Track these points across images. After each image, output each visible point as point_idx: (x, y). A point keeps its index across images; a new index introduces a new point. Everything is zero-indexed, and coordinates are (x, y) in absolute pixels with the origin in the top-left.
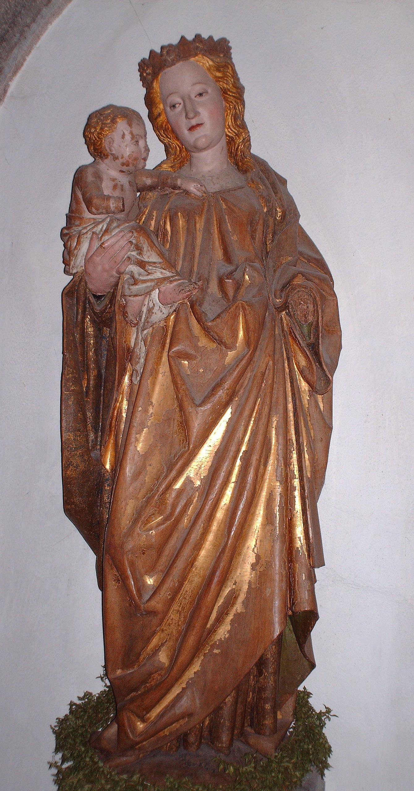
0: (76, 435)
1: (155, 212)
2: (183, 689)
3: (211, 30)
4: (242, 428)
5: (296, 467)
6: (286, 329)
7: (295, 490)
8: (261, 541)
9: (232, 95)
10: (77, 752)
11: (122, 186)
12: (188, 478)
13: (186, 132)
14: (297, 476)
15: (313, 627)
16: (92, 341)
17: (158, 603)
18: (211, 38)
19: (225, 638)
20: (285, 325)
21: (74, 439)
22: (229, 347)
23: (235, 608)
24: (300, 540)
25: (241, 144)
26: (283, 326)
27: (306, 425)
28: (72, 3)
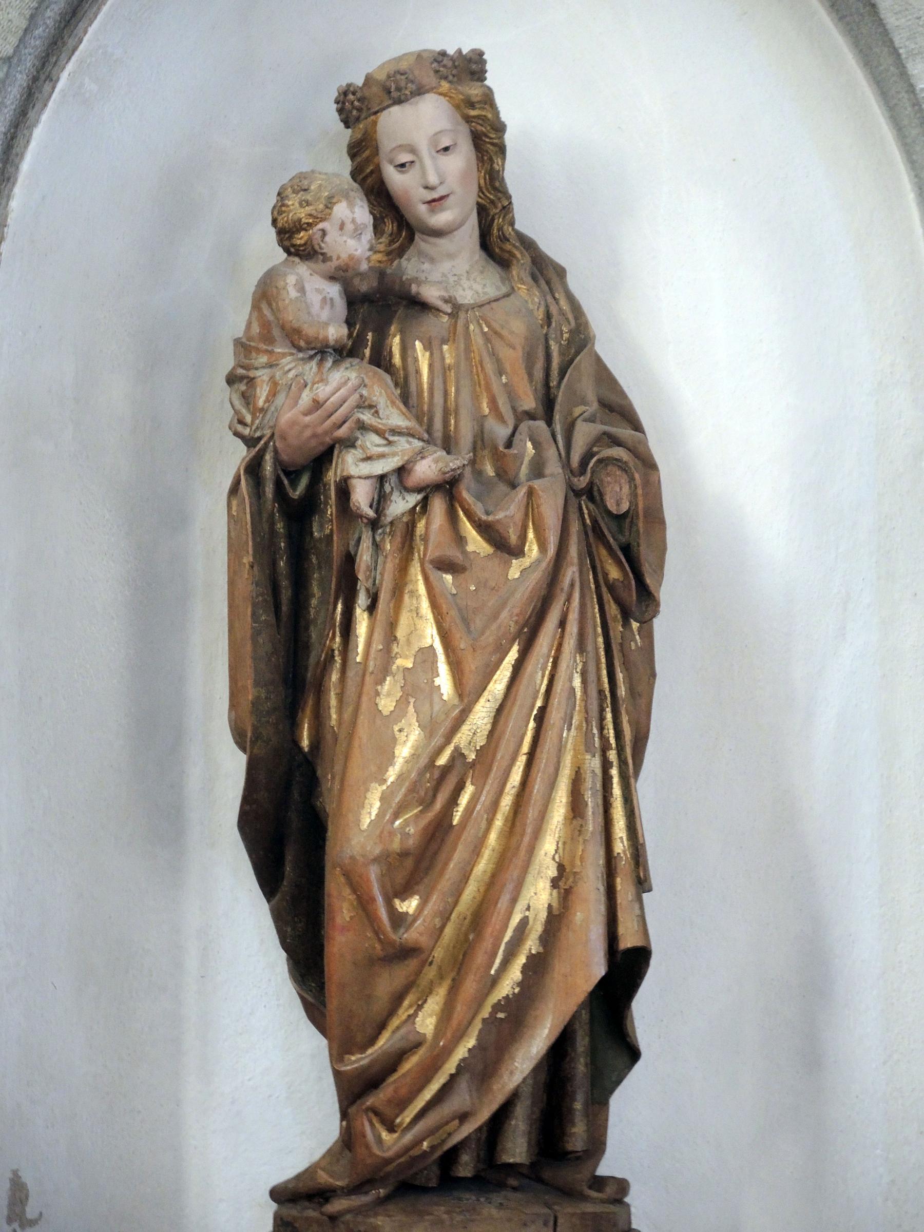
0: (268, 692)
1: (370, 334)
2: (452, 1076)
3: (456, 40)
5: (612, 732)
6: (588, 521)
7: (611, 767)
8: (564, 843)
9: (486, 137)
11: (331, 299)
12: (457, 749)
13: (423, 209)
14: (614, 746)
16: (282, 544)
17: (421, 934)
19: (514, 993)
20: (586, 516)
21: (266, 698)
22: (519, 552)
24: (622, 842)
25: (497, 216)
26: (583, 519)
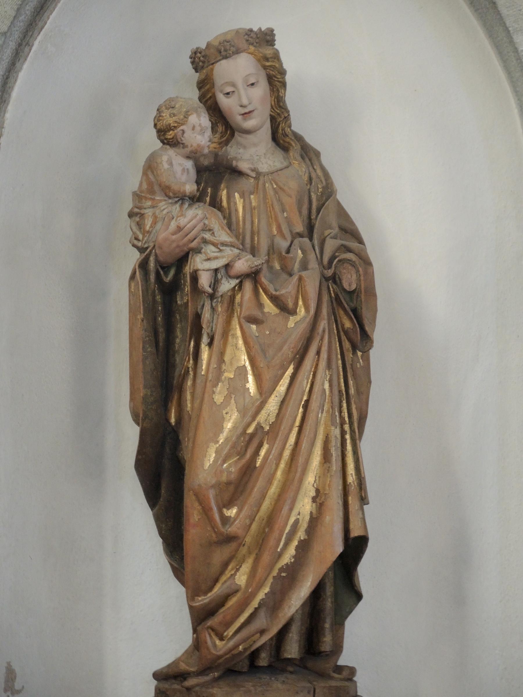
4: (306, 381)
5: (346, 414)
6: (333, 295)
7: (346, 434)
8: (319, 477)
10: (181, 663)
14: (347, 422)
15: (350, 612)
18: (260, 29)
19: (291, 562)
20: (332, 292)
23: (298, 536)
24: (352, 476)
25: (281, 122)
27: (354, 375)
28: (61, 2)
